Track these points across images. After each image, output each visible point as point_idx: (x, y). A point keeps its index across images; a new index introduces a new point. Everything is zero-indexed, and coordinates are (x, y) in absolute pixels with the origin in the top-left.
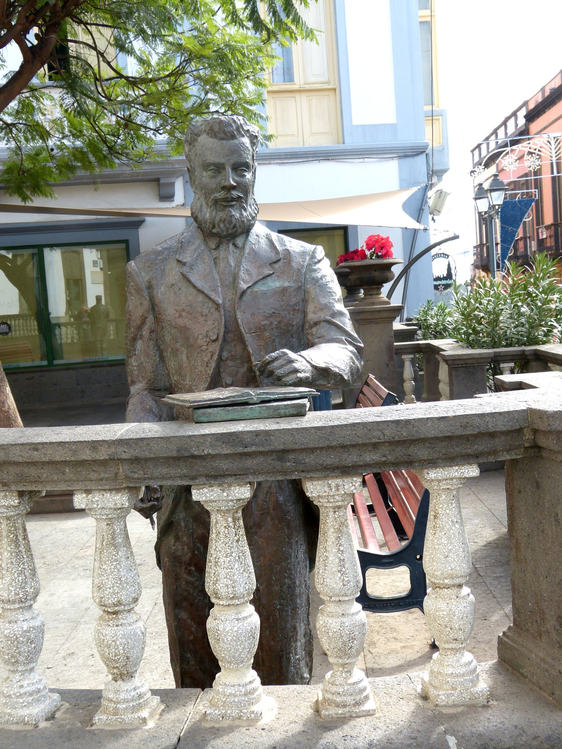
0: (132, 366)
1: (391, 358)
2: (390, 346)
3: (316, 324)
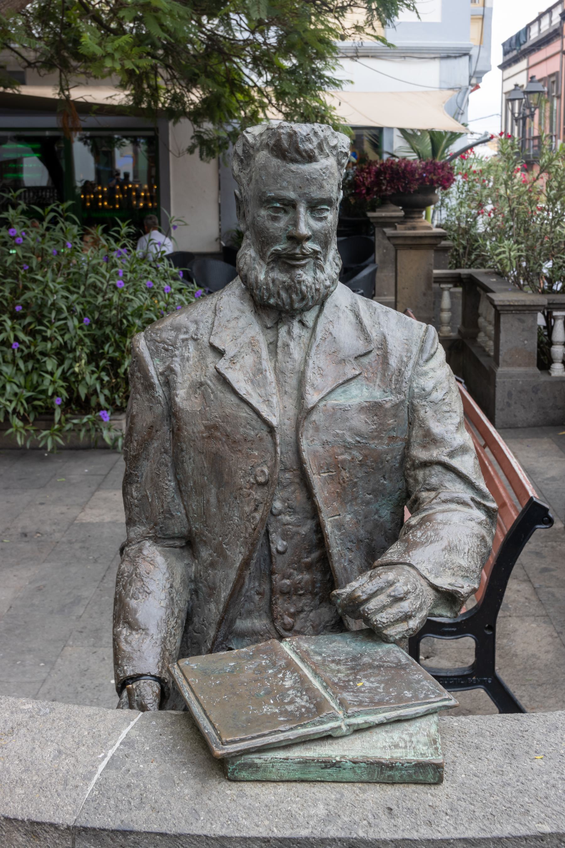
0: (132, 497)
1: (429, 287)
2: (430, 273)
3: (426, 464)
